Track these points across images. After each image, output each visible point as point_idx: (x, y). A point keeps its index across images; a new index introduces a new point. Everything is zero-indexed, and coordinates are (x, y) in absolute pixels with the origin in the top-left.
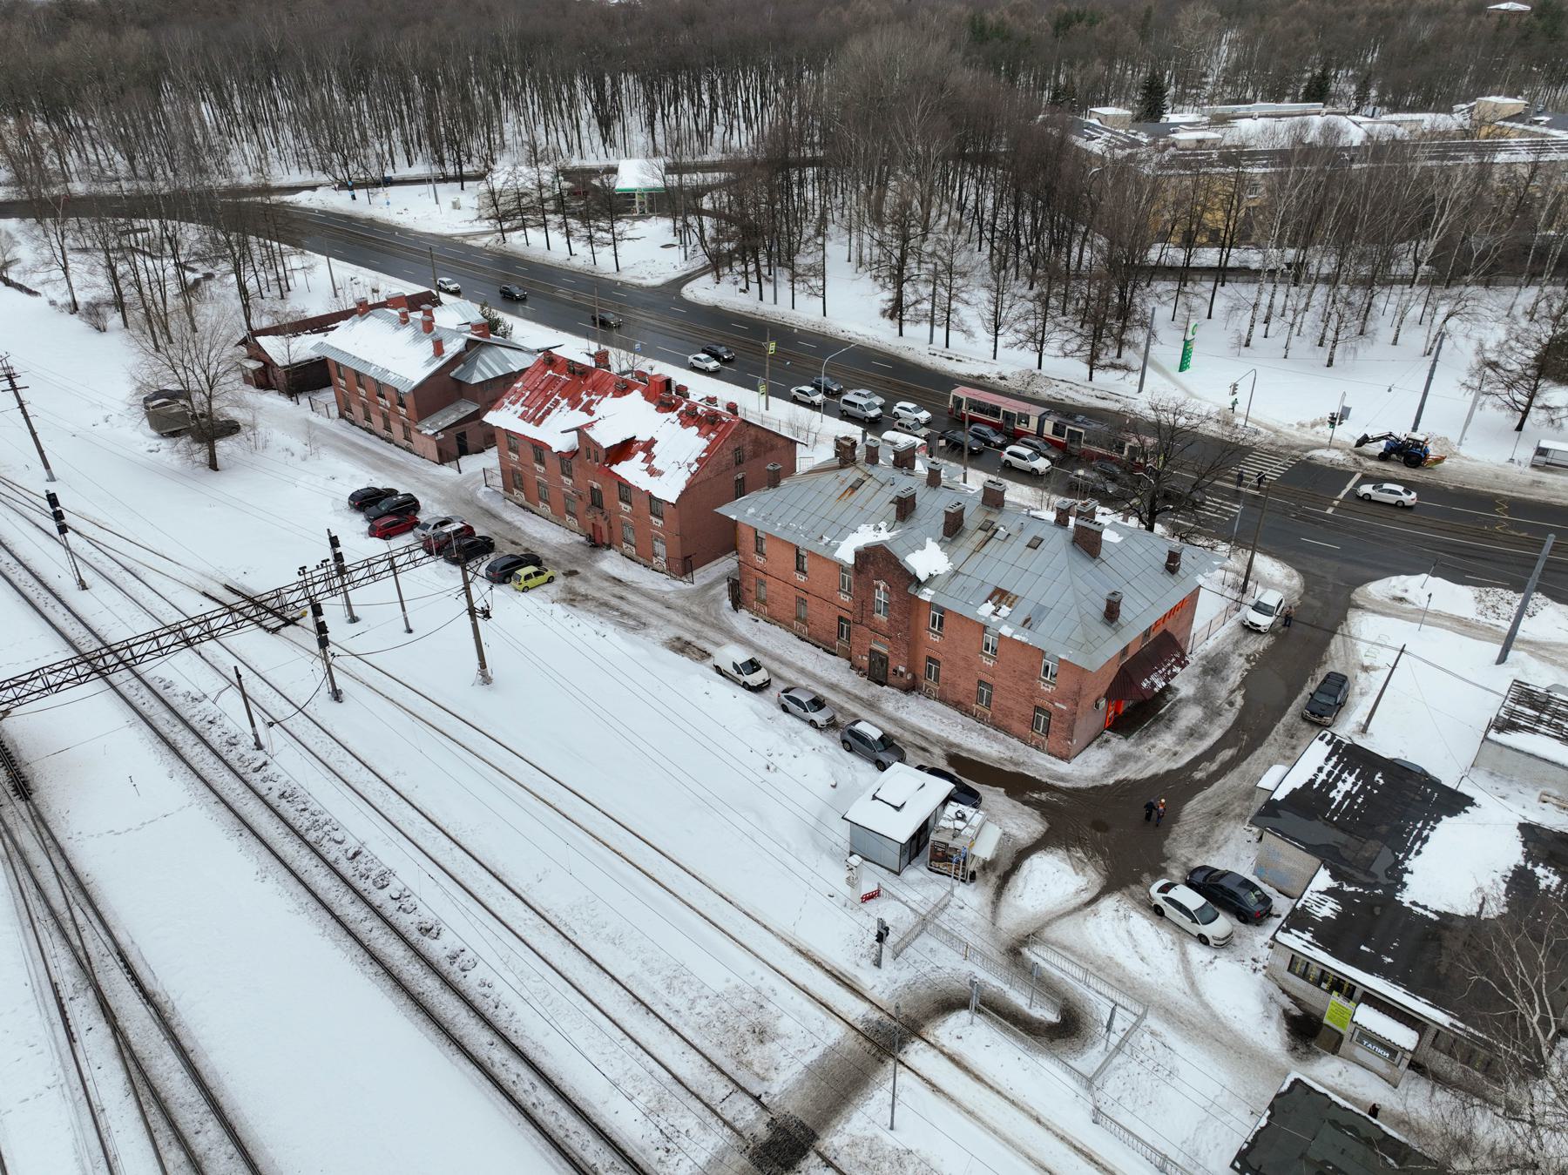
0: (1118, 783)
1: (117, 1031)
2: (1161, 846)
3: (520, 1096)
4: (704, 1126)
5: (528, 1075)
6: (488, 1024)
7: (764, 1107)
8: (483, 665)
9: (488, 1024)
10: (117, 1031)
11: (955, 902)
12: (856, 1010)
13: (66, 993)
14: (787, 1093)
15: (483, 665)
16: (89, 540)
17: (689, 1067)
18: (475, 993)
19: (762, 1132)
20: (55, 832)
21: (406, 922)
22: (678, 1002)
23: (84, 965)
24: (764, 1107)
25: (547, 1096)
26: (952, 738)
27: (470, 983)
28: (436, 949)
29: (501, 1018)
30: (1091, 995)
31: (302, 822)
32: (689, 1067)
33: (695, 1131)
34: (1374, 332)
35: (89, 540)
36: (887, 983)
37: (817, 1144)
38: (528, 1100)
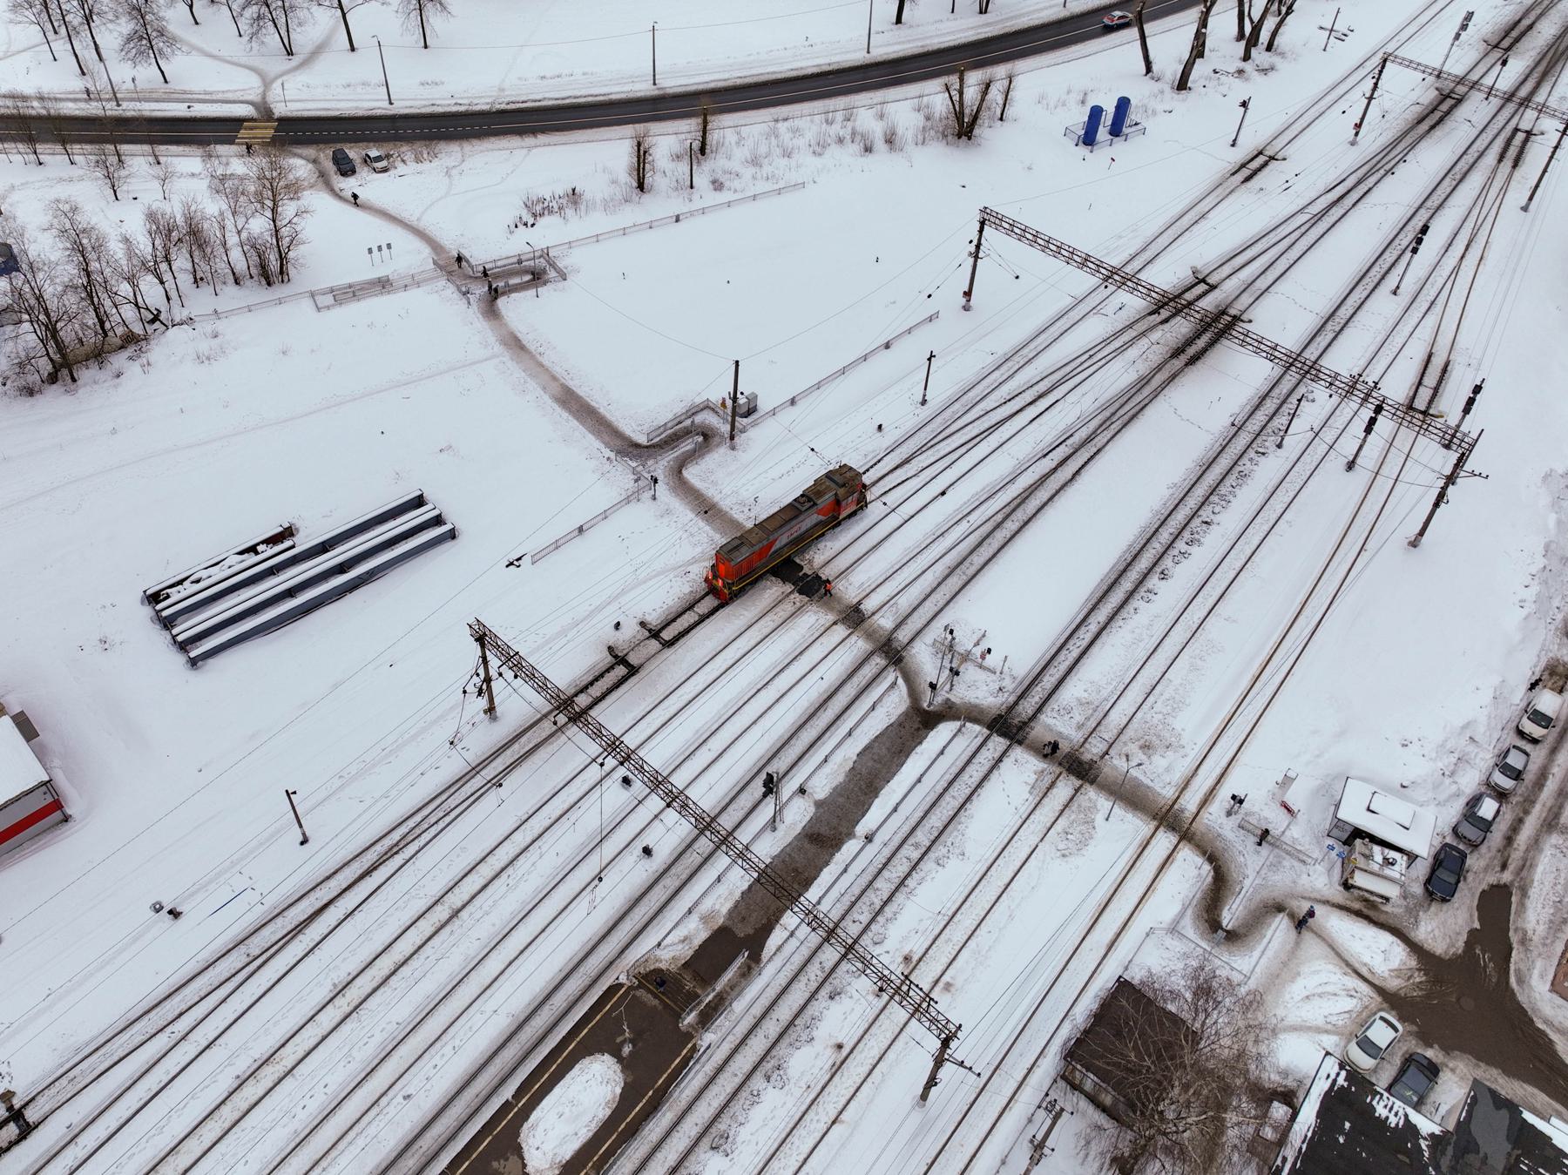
0: (1543, 1033)
1: (1055, 470)
2: (1463, 1050)
3: (1071, 642)
4: (1080, 727)
5: (1085, 643)
6: (1111, 619)
7: (1102, 757)
8: (1422, 533)
9: (1111, 619)
10: (1055, 470)
11: (1311, 868)
12: (1190, 803)
13: (1069, 442)
14: (1115, 768)
15: (1422, 533)
16: (1457, 269)
17: (1117, 718)
18: (1130, 607)
19: (1087, 757)
20: (1423, 144)
21: (1167, 562)
22: (1158, 707)
23: (1088, 440)
24: (1102, 757)
25: (1075, 653)
26: (1534, 892)
27: (1136, 602)
28: (1153, 581)
29: (1118, 622)
30: (1256, 954)
31: (1223, 490)
32: (1117, 718)
33: (1074, 721)
34: (720, 144)
35: (1457, 269)
36: (1215, 817)
37: (1087, 786)
38: (1070, 645)
